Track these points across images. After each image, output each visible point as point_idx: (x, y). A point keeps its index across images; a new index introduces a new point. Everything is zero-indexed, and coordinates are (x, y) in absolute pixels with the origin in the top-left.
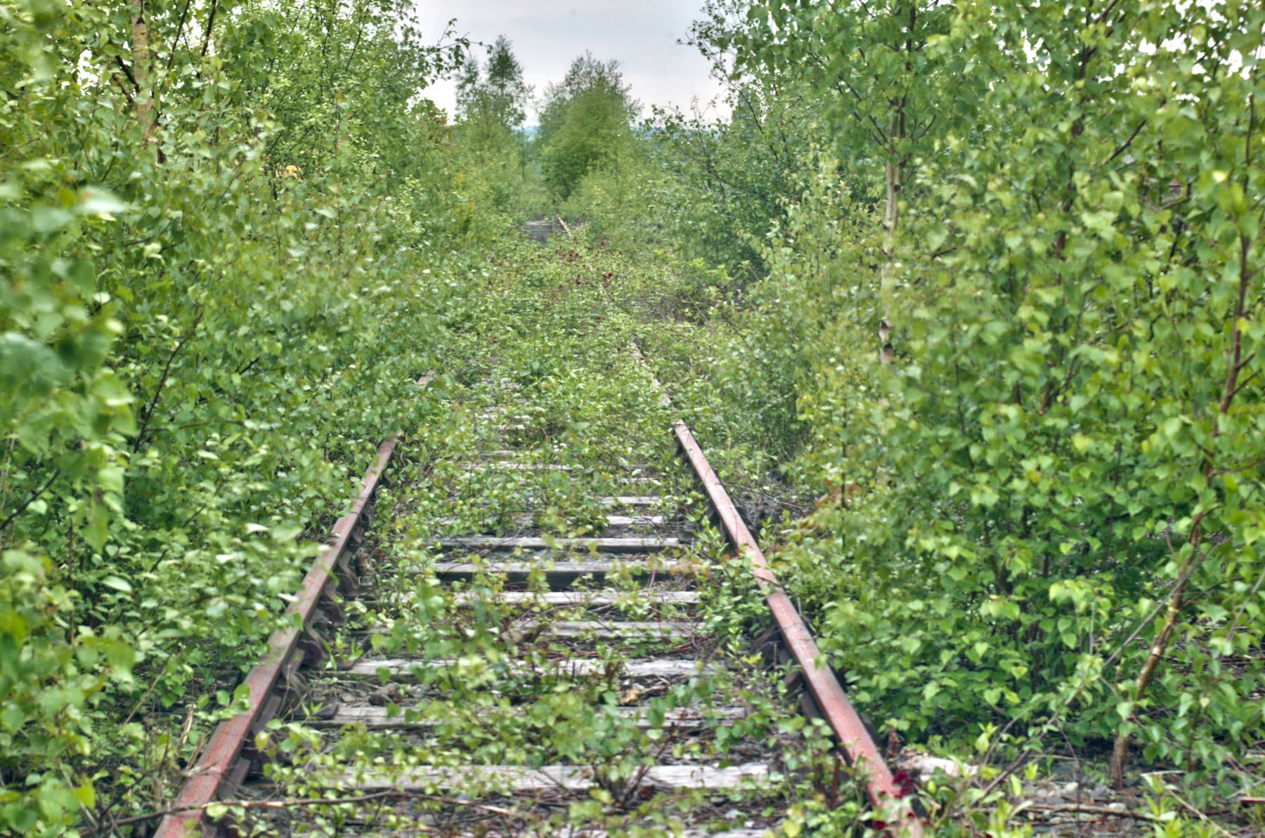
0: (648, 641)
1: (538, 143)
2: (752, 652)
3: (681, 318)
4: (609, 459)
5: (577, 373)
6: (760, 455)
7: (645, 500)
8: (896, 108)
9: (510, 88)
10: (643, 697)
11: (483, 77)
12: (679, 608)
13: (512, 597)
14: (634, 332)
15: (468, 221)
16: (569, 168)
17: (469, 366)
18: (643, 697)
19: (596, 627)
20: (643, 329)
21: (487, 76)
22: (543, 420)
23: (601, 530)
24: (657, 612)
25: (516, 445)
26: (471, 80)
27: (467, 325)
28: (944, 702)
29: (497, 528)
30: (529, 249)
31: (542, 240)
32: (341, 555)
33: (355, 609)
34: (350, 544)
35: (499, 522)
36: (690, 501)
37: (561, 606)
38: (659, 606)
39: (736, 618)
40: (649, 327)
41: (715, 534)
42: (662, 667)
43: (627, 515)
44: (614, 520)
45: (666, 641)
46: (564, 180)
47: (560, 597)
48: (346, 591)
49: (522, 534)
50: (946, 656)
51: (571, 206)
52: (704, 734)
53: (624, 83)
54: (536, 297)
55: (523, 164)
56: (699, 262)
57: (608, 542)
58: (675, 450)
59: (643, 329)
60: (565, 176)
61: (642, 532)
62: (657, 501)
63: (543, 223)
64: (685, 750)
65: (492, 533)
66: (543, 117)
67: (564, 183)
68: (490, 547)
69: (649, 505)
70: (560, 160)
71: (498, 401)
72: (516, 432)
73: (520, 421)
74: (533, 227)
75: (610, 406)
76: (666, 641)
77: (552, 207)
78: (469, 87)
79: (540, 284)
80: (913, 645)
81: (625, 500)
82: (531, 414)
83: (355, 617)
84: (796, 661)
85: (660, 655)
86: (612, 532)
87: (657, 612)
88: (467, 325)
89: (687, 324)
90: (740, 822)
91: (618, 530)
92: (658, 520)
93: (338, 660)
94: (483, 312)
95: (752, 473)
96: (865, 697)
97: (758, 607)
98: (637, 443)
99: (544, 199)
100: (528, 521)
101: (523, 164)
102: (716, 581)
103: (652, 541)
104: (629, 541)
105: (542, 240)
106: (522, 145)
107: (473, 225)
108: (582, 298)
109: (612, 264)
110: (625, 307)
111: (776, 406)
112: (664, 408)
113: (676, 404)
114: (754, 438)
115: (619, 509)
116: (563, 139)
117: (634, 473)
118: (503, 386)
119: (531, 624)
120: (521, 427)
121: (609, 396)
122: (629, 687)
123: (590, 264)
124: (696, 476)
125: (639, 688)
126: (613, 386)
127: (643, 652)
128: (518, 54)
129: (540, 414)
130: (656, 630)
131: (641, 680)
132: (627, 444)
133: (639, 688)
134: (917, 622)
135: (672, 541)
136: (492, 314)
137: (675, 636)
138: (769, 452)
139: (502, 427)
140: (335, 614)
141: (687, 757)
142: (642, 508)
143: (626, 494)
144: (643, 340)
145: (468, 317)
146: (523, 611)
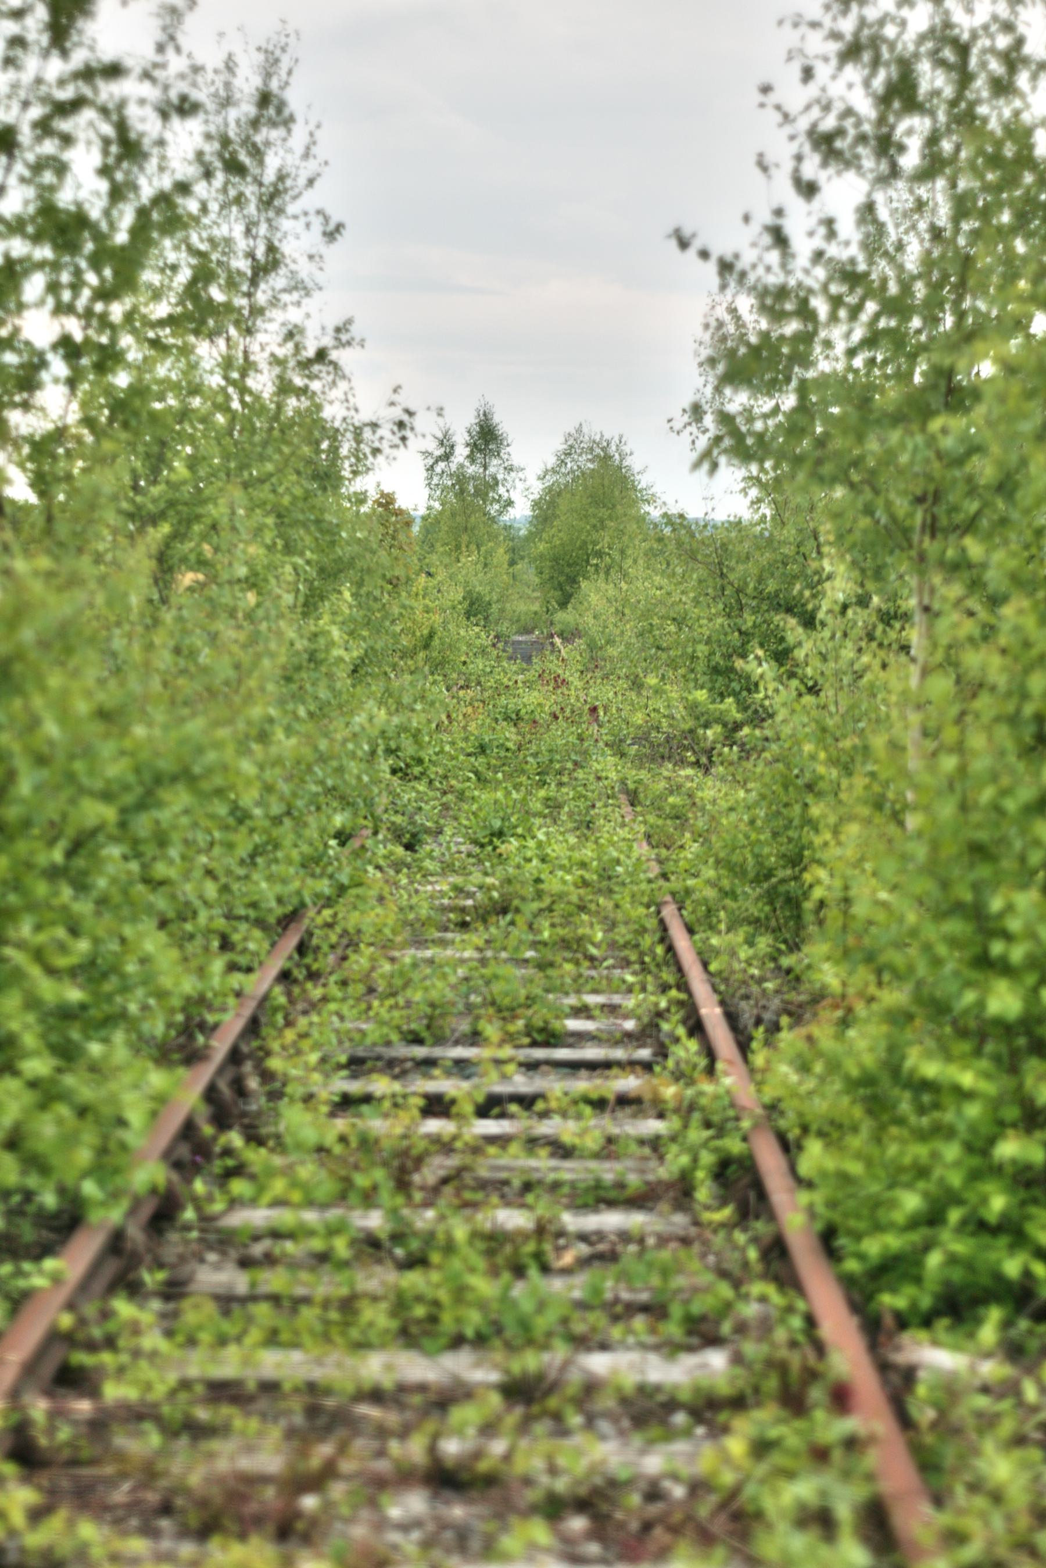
0: (598, 1185)
1: (531, 537)
2: (723, 1202)
3: (682, 762)
4: (575, 945)
5: (547, 834)
6: (764, 943)
7: (616, 999)
8: (925, 506)
9: (495, 467)
10: (584, 1263)
11: (461, 453)
12: (642, 1142)
13: (434, 1126)
14: (623, 782)
15: (431, 636)
16: (567, 570)
17: (413, 823)
18: (584, 1263)
19: (542, 1163)
20: (633, 775)
21: (467, 451)
22: (495, 894)
23: (550, 1038)
24: (609, 1150)
25: (464, 925)
26: (446, 457)
27: (417, 770)
28: (957, 1275)
29: (425, 1034)
30: (510, 671)
31: (528, 659)
32: (220, 1071)
33: (230, 1142)
34: (235, 1057)
35: (429, 1027)
36: (663, 1004)
37: (492, 1140)
38: (610, 1140)
39: (707, 1158)
40: (643, 774)
41: (693, 1045)
42: (611, 1220)
43: (590, 1017)
44: (573, 1024)
45: (620, 1185)
46: (560, 584)
47: (490, 1127)
48: (222, 1120)
49: (457, 1043)
50: (954, 1215)
51: (565, 617)
52: (656, 1310)
53: (635, 463)
54: (510, 735)
55: (512, 563)
56: (701, 695)
57: (562, 1054)
58: (657, 936)
59: (633, 775)
60: (562, 579)
61: (608, 1041)
62: (630, 1003)
63: (532, 637)
64: (630, 1331)
65: (418, 1041)
66: (536, 504)
67: (560, 587)
68: (413, 1059)
69: (620, 1006)
70: (555, 559)
71: (448, 868)
72: (463, 910)
73: (470, 895)
74: (520, 642)
75: (582, 877)
76: (620, 1185)
77: (545, 617)
78: (441, 466)
79: (515, 719)
80: (911, 1202)
81: (591, 999)
82: (481, 887)
83: (228, 1152)
84: (772, 1216)
85: (611, 1204)
86: (571, 1040)
87: (609, 1150)
88: (417, 770)
89: (689, 771)
90: (687, 1433)
91: (580, 1038)
92: (630, 1025)
93: (198, 1209)
94: (437, 754)
95: (750, 965)
96: (852, 1265)
97: (734, 1146)
98: (612, 926)
99: (536, 607)
100: (464, 1026)
101: (512, 563)
102: (688, 1110)
103: (619, 1054)
104: (591, 1053)
105: (528, 659)
106: (512, 540)
107: (436, 642)
108: (561, 736)
109: (604, 693)
110: (618, 747)
111: (783, 881)
112: (650, 881)
113: (665, 876)
114: (756, 922)
115: (582, 1011)
116: (557, 535)
117: (605, 964)
118: (454, 849)
119: (453, 1161)
120: (470, 902)
121: (583, 865)
122: (565, 1248)
123: (577, 692)
124: (680, 970)
125: (584, 1249)
126: (588, 853)
127: (590, 1200)
128: (504, 423)
129: (490, 888)
130: (608, 1172)
131: (583, 1237)
132: (597, 927)
133: (584, 1249)
134: (922, 1172)
135: (644, 1053)
136: (453, 758)
137: (634, 1180)
138: (776, 939)
139: (446, 901)
140: (202, 1150)
141: (631, 1340)
142: (612, 1009)
143: (595, 991)
144: (635, 792)
145: (420, 761)
146: (445, 1146)
